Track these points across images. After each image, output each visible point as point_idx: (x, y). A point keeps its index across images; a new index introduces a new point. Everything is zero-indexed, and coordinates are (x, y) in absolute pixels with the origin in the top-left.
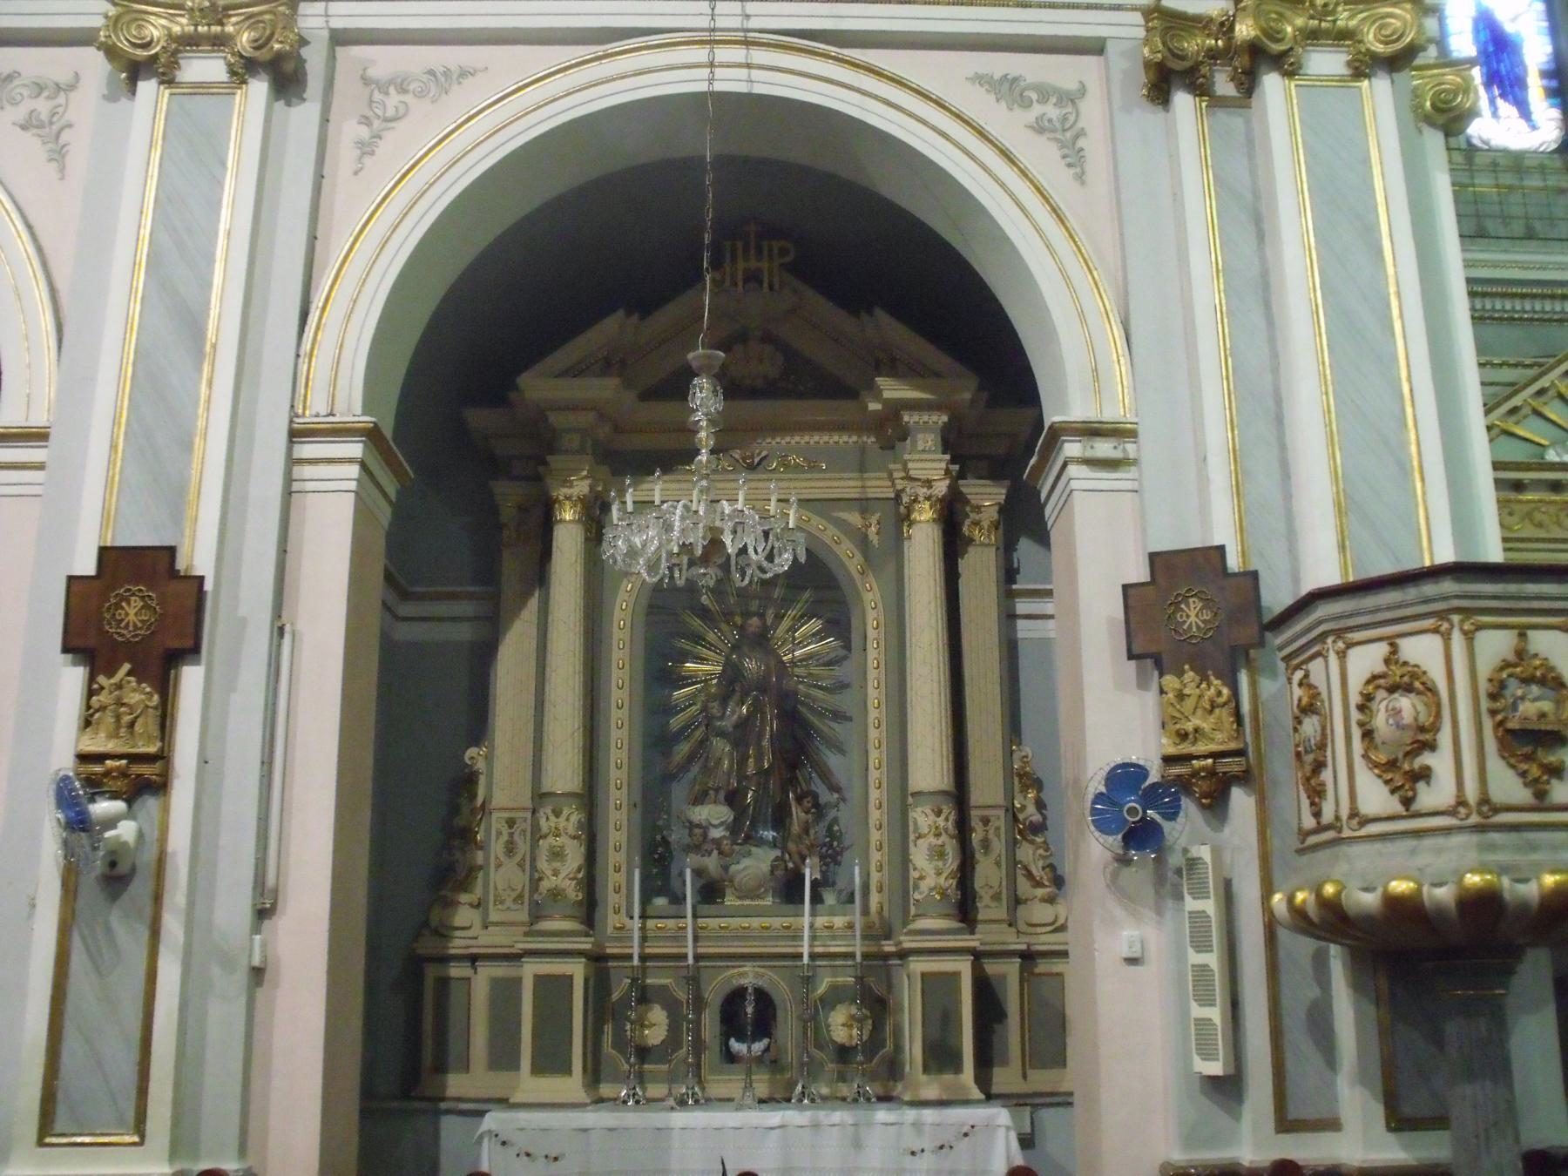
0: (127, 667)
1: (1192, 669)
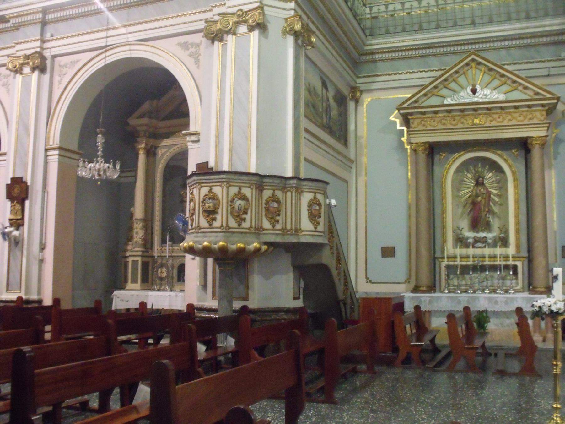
0: (16, 202)
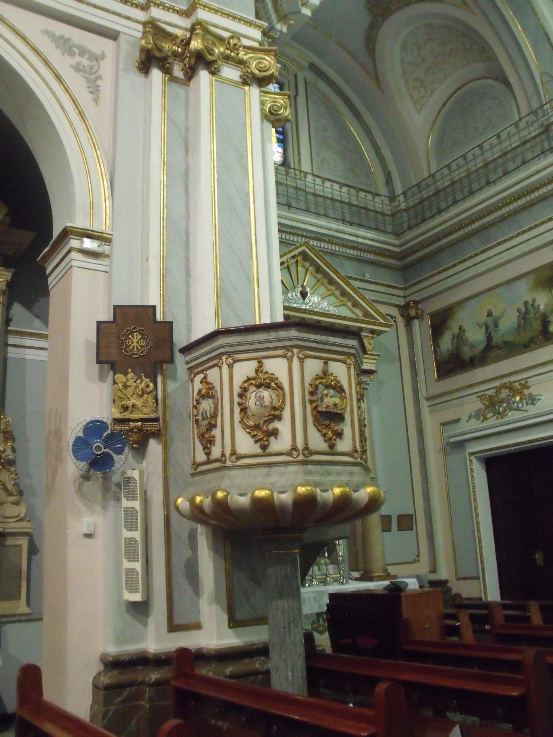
1: (132, 372)
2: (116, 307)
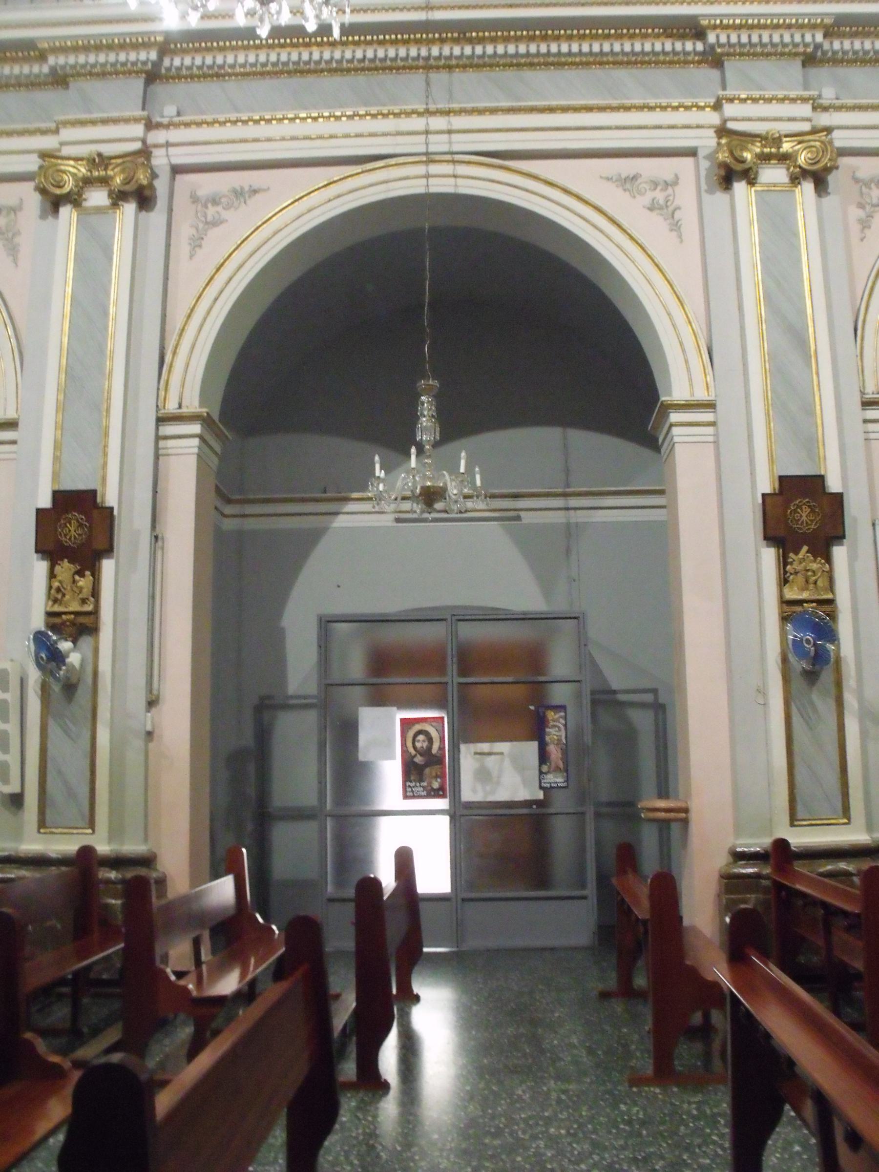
0: (805, 548)
2: (781, 478)
